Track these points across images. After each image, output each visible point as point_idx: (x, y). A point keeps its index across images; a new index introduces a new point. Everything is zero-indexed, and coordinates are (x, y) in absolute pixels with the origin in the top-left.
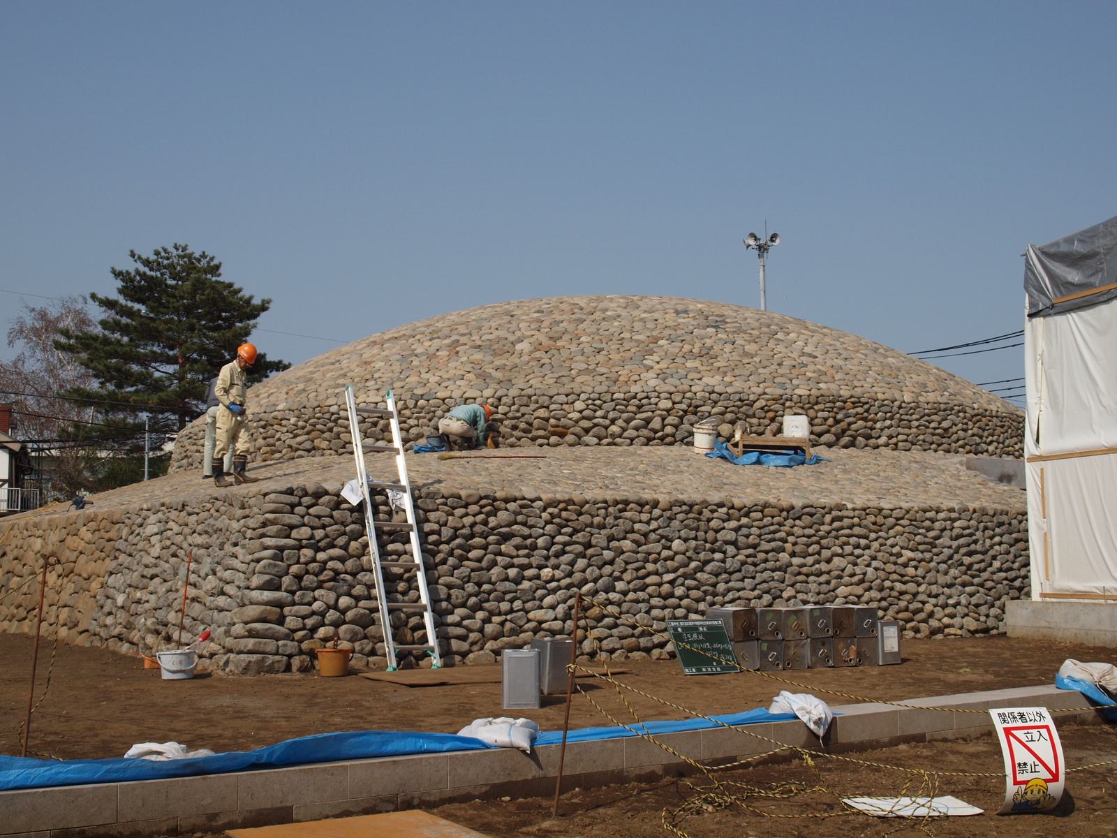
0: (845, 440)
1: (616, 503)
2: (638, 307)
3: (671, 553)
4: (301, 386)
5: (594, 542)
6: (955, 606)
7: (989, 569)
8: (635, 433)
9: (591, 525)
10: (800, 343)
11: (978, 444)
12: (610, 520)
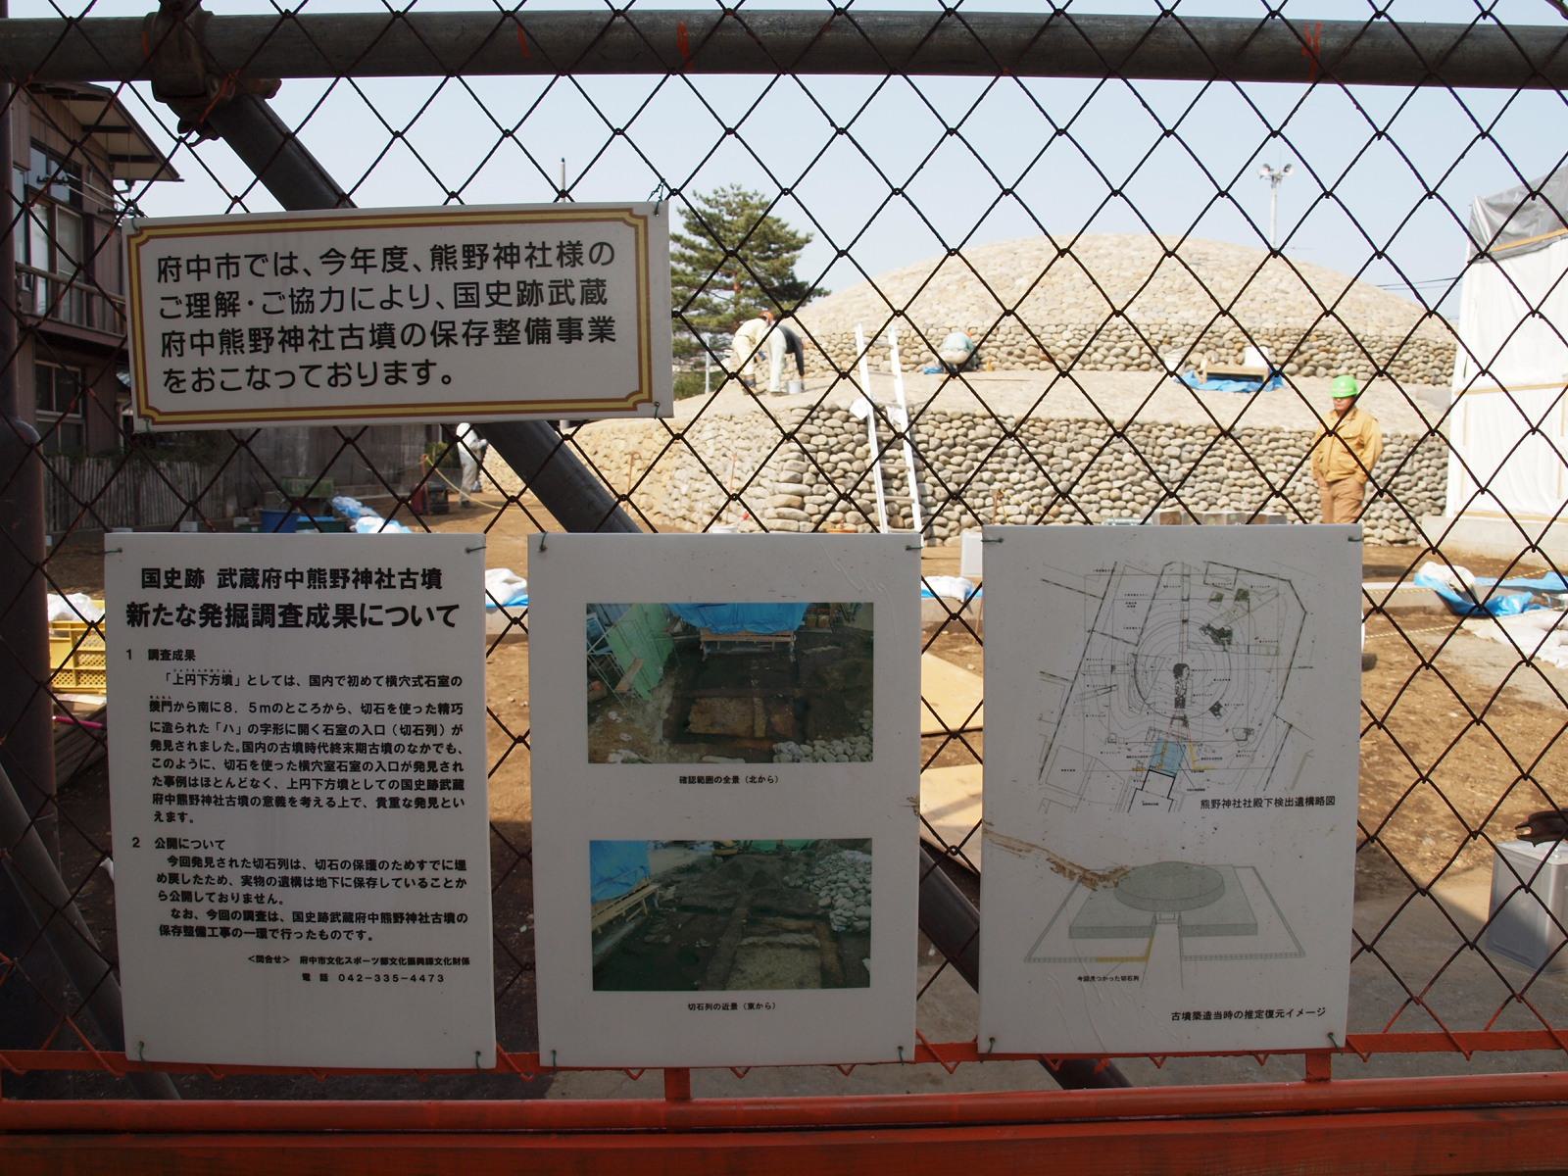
0: (1307, 369)
1: (1077, 421)
2: (1129, 245)
3: (1121, 464)
4: (832, 315)
5: (1055, 453)
6: (1377, 519)
7: (1415, 489)
8: (1115, 360)
9: (1055, 439)
10: (1276, 280)
11: (1437, 376)
12: (1071, 435)
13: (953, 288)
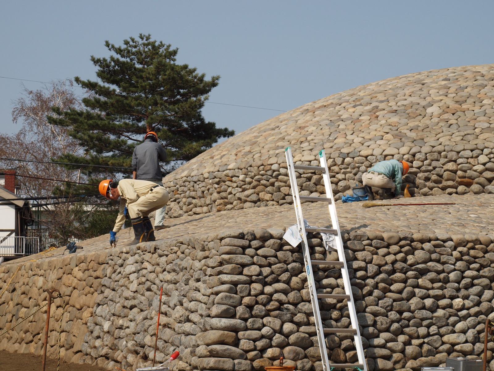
4: (247, 149)
13: (365, 118)
